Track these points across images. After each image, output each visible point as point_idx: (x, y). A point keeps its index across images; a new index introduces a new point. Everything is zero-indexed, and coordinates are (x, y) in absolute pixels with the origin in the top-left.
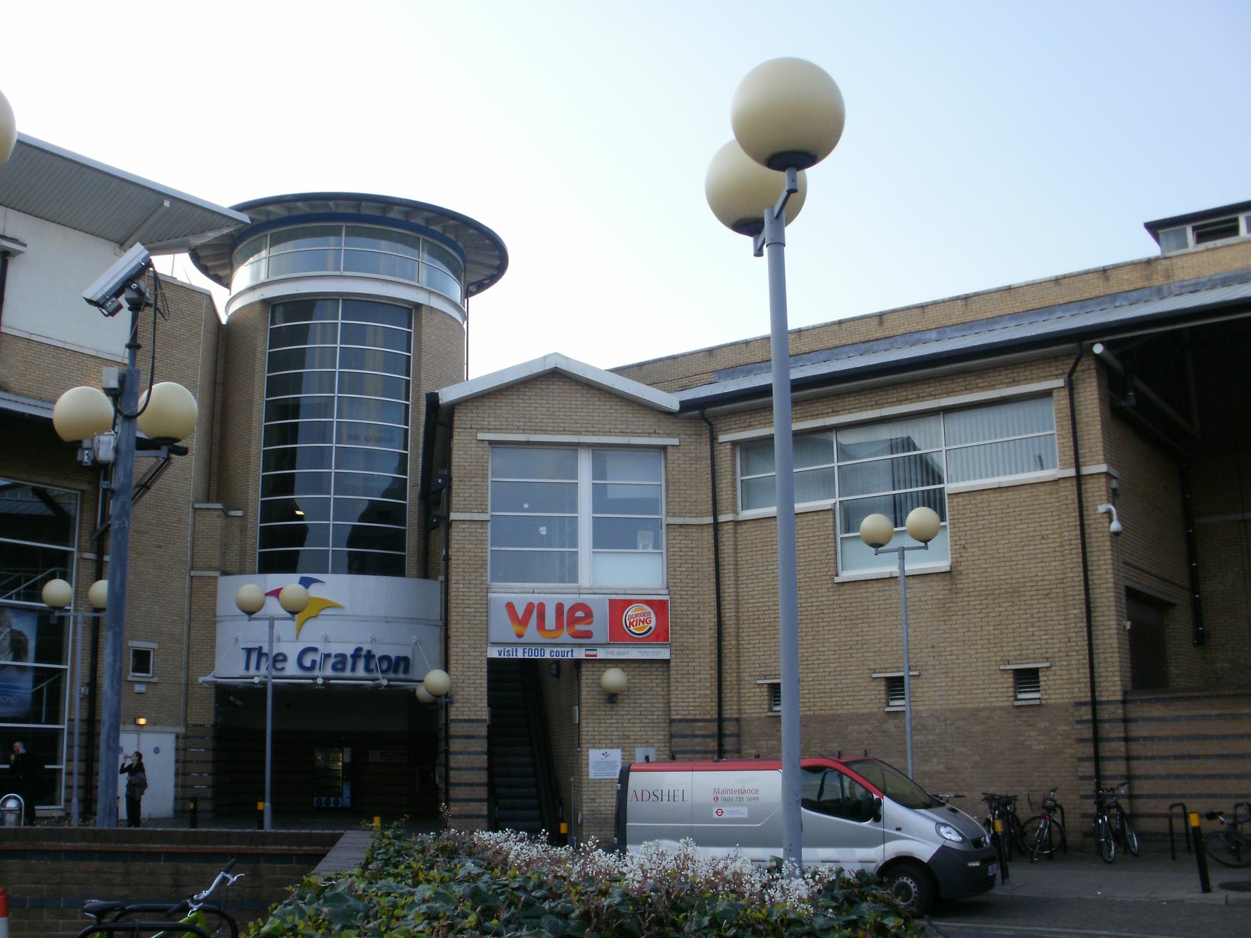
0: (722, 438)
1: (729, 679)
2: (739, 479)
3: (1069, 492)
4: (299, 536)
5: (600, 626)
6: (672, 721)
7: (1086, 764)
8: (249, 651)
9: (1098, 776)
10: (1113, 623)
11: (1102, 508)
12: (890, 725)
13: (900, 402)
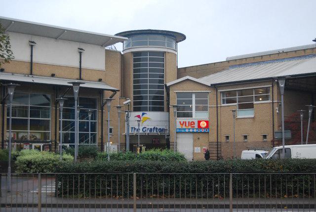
5: (196, 126)
8: (132, 128)
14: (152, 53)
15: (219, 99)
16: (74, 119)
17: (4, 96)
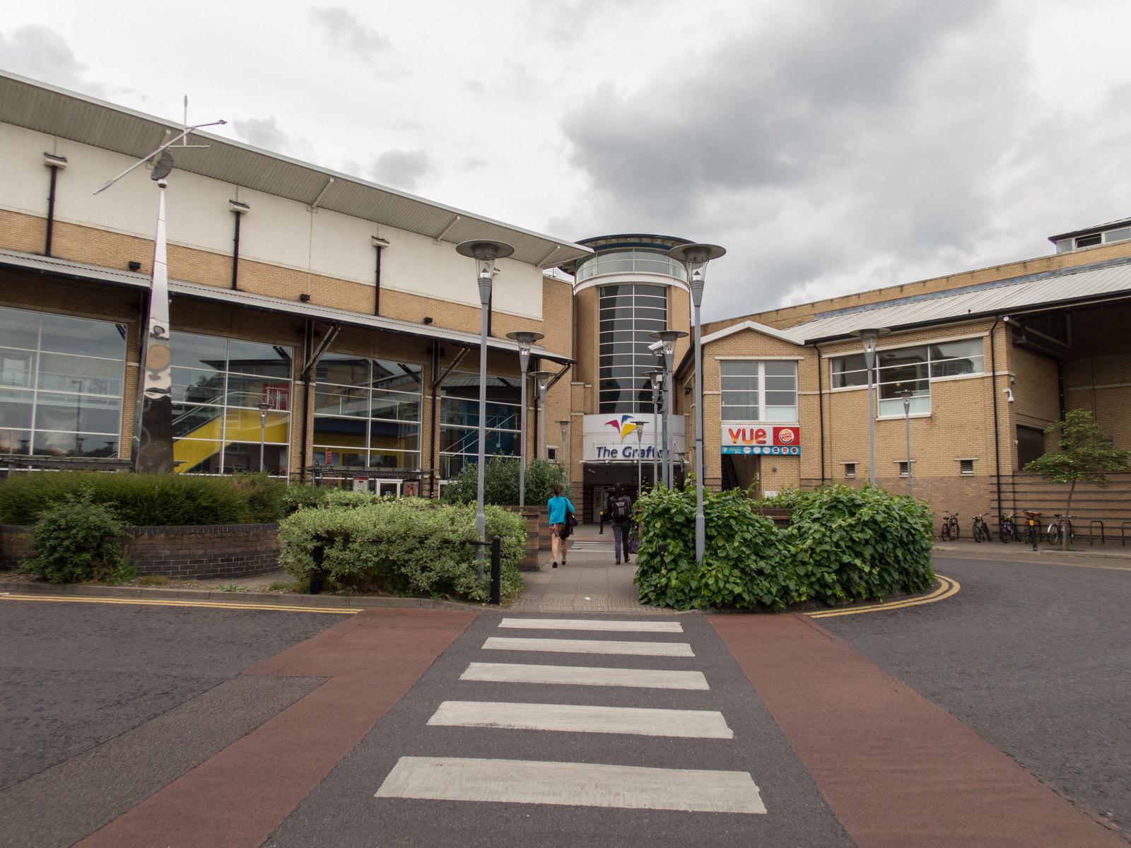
0: (823, 356)
1: (827, 461)
2: (832, 374)
3: (989, 383)
4: (616, 396)
5: (769, 439)
6: (801, 479)
7: (994, 502)
8: (600, 449)
9: (1000, 508)
10: (1009, 442)
11: (1005, 390)
12: (902, 483)
13: (909, 341)
14: (641, 287)
15: (824, 377)
16: (478, 425)
17: (308, 359)
